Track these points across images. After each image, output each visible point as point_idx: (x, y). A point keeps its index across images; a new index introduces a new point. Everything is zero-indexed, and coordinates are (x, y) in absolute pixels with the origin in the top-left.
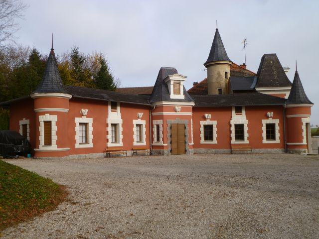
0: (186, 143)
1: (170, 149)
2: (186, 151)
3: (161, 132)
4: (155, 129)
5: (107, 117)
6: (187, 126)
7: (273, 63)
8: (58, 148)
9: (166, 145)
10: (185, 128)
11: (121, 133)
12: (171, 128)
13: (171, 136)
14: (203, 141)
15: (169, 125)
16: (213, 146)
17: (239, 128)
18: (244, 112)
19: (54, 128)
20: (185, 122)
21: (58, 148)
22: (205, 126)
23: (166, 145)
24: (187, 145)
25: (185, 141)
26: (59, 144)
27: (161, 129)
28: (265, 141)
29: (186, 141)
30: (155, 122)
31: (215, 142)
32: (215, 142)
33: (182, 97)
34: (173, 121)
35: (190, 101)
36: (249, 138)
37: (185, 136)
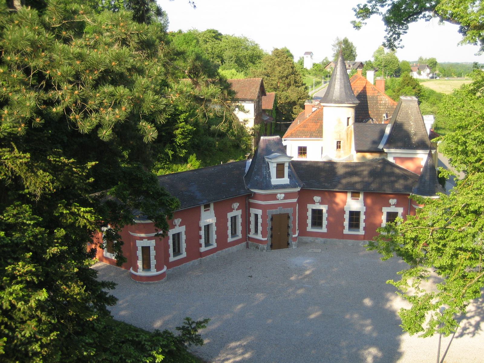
0: (288, 234)
1: (270, 243)
2: (288, 244)
3: (259, 224)
4: (252, 219)
5: (199, 219)
6: (291, 215)
7: (412, 113)
8: (157, 271)
9: (266, 239)
10: (289, 217)
11: (214, 232)
12: (272, 219)
13: (272, 229)
14: (309, 229)
15: (270, 217)
16: (322, 235)
17: (354, 216)
18: (361, 196)
19: (153, 253)
20: (289, 210)
21: (157, 271)
22: (314, 211)
23: (266, 239)
24: (290, 238)
25: (288, 225)
26: (158, 268)
27: (260, 220)
28: (346, 231)
29: (290, 233)
30: (253, 211)
31: (324, 230)
32: (324, 230)
33: (286, 180)
34: (275, 211)
35: (295, 187)
36: (365, 228)
37: (289, 227)
